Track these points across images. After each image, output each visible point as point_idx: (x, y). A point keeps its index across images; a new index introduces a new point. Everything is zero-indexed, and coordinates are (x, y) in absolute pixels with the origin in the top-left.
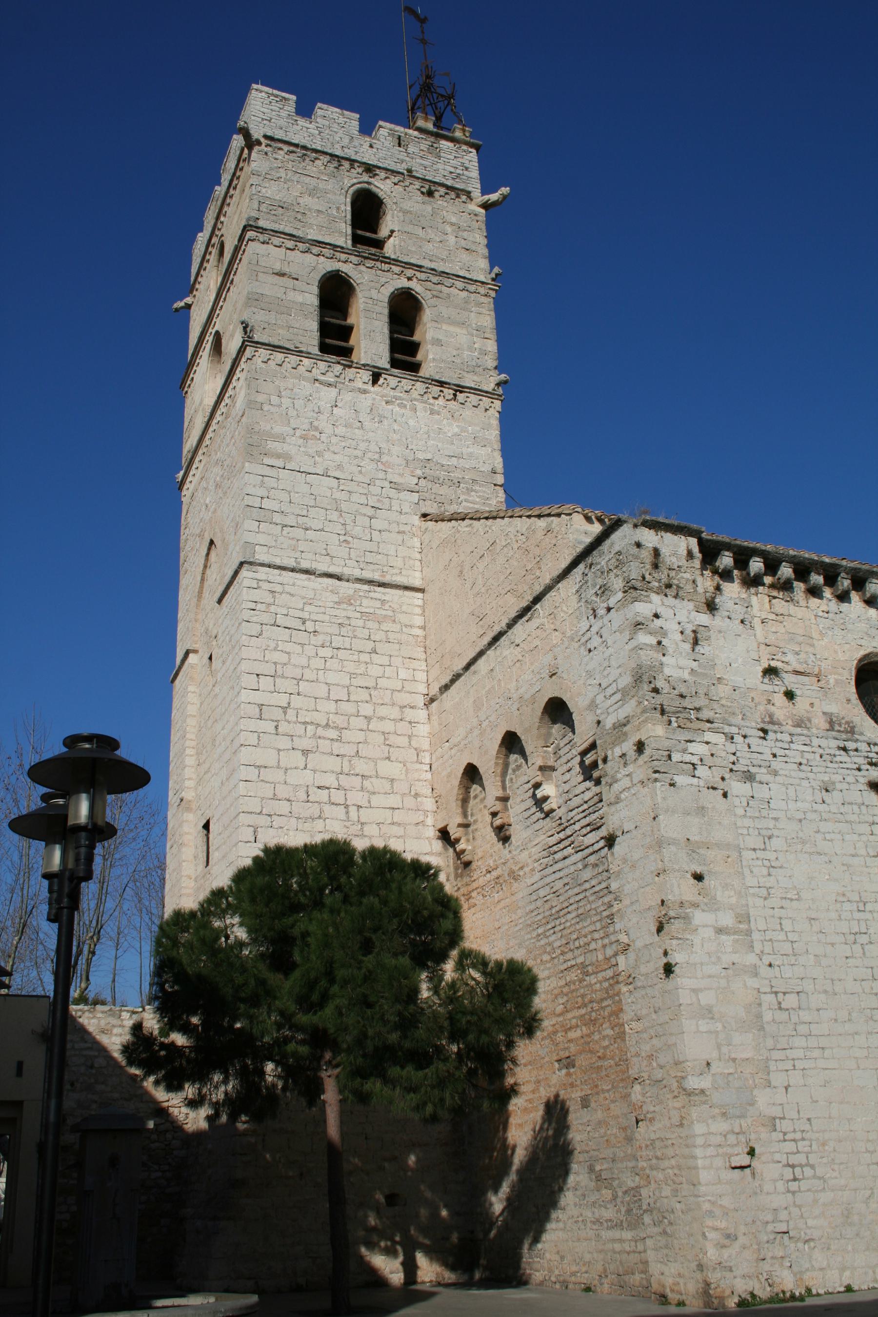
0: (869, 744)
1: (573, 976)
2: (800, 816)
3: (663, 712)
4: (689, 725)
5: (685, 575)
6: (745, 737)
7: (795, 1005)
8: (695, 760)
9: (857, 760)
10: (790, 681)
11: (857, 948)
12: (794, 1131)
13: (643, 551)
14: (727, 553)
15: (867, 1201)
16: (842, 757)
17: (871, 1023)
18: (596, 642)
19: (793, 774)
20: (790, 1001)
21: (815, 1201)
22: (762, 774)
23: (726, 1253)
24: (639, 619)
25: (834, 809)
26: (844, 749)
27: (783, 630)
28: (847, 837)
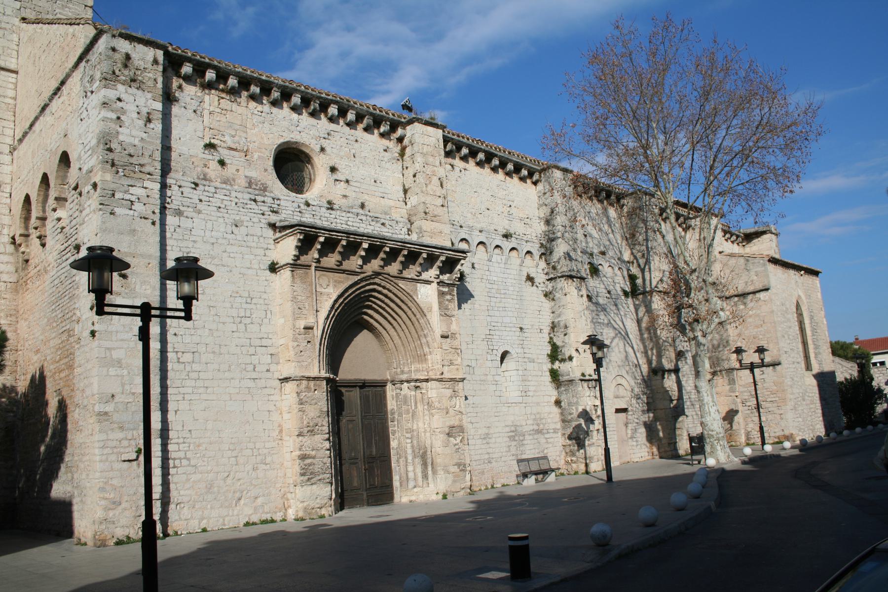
0: (274, 199)
1: (64, 337)
2: (214, 240)
3: (113, 165)
4: (132, 175)
5: (149, 75)
6: (180, 187)
7: (190, 360)
8: (133, 198)
9: (262, 208)
10: (224, 153)
11: (242, 326)
12: (178, 438)
13: (116, 54)
14: (188, 64)
15: (225, 479)
16: (253, 205)
17: (244, 372)
18: (84, 115)
19: (213, 213)
20: (187, 357)
21: (188, 480)
22: (189, 212)
23: (111, 514)
24: (106, 101)
25: (239, 238)
26: (255, 201)
27: (225, 120)
28: (246, 256)
